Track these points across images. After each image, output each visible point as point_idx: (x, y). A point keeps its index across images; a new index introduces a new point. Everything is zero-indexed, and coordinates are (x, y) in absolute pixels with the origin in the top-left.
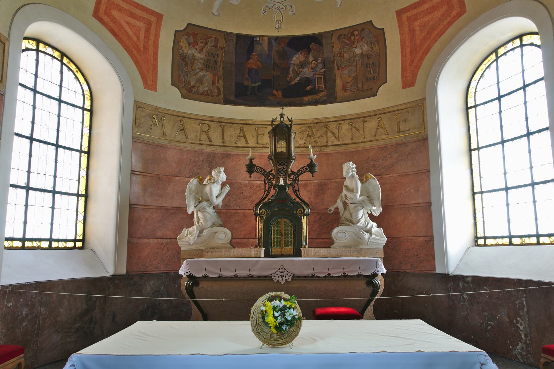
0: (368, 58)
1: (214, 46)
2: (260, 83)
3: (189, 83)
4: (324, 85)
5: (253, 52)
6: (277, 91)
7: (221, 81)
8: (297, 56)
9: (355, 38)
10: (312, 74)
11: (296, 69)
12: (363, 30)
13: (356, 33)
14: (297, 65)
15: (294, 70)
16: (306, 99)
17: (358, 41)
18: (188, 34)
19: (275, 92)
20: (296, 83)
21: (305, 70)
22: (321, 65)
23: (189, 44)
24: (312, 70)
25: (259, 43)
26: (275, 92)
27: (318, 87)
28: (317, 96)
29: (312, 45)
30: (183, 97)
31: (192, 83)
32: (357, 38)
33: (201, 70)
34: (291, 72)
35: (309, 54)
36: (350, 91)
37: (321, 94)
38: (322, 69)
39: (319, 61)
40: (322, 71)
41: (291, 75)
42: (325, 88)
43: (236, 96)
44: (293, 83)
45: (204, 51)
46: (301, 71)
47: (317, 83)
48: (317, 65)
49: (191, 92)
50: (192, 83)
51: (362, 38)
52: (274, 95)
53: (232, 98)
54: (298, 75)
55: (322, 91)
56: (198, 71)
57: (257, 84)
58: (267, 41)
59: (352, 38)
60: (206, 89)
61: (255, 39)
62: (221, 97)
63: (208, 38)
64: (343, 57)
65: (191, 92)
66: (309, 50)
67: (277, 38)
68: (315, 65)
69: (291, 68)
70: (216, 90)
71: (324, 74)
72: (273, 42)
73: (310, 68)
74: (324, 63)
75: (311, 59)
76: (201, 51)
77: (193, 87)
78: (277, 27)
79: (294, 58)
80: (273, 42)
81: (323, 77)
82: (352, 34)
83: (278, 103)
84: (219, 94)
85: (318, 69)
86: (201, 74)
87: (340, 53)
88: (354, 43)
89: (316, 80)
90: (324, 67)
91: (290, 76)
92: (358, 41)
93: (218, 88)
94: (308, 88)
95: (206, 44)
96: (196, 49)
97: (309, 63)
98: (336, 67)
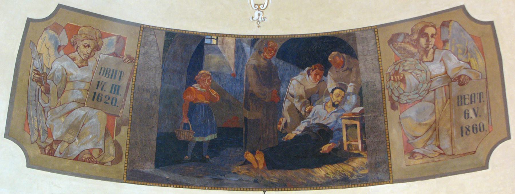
0: (462, 84)
1: (114, 54)
2: (214, 136)
3: (49, 133)
4: (363, 142)
5: (201, 68)
6: (254, 153)
7: (124, 130)
8: (299, 78)
9: (428, 41)
10: (333, 118)
11: (298, 105)
12: (445, 24)
13: (430, 31)
14: (301, 97)
15: (292, 108)
16: (321, 172)
17: (435, 48)
18: (57, 28)
19: (249, 156)
20: (297, 137)
21: (318, 108)
22: (353, 99)
23: (59, 48)
24: (335, 109)
25: (215, 49)
26: (249, 156)
27: (349, 145)
28: (346, 167)
29: (334, 56)
30: (31, 164)
31: (57, 134)
32: (433, 41)
33: (81, 104)
34: (285, 113)
35: (326, 74)
36: (424, 156)
37: (356, 163)
38: (356, 106)
39: (350, 88)
40: (357, 110)
41: (286, 118)
42: (365, 149)
43: (158, 164)
44: (291, 136)
45: (92, 63)
46: (310, 111)
47: (345, 138)
48: (344, 99)
49: (51, 153)
50: (57, 134)
51: (445, 42)
52: (247, 162)
53: (149, 168)
54: (302, 118)
55: (359, 155)
56: (72, 106)
57: (208, 138)
58: (233, 47)
59: (423, 41)
60: (90, 146)
61: (207, 41)
62: (122, 166)
63: (102, 38)
64: (403, 80)
65: (51, 153)
66: (326, 66)
67: (254, 40)
68: (339, 99)
69: (286, 104)
70: (112, 150)
71: (361, 117)
72: (248, 49)
73: (329, 104)
74: (360, 94)
75: (331, 84)
76: (84, 63)
77: (57, 142)
78: (256, 17)
79: (294, 82)
80: (248, 49)
81: (358, 123)
82: (422, 33)
83: (256, 181)
84: (118, 159)
85: (347, 107)
86: (81, 112)
87: (397, 73)
88: (426, 52)
89: (344, 130)
90: (361, 102)
91: (283, 121)
92: (435, 48)
93: (117, 145)
94: (325, 148)
95: (97, 48)
96: (73, 59)
97: (327, 94)
98: (388, 104)
